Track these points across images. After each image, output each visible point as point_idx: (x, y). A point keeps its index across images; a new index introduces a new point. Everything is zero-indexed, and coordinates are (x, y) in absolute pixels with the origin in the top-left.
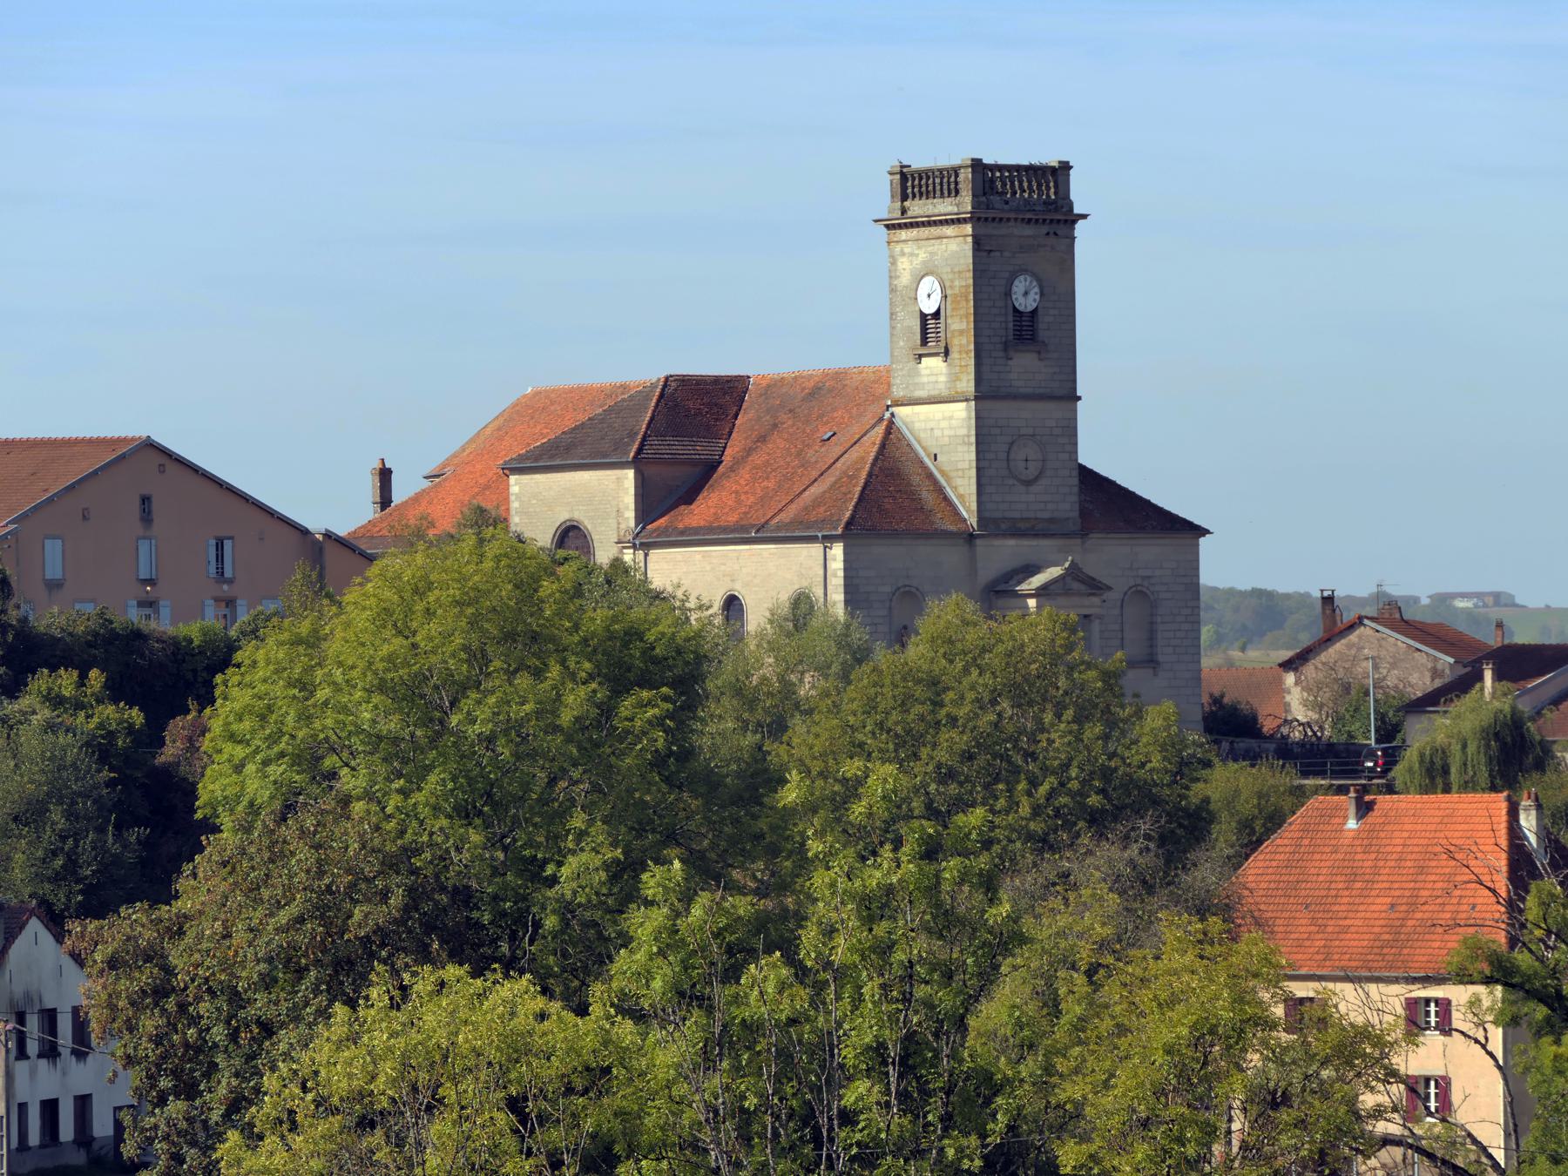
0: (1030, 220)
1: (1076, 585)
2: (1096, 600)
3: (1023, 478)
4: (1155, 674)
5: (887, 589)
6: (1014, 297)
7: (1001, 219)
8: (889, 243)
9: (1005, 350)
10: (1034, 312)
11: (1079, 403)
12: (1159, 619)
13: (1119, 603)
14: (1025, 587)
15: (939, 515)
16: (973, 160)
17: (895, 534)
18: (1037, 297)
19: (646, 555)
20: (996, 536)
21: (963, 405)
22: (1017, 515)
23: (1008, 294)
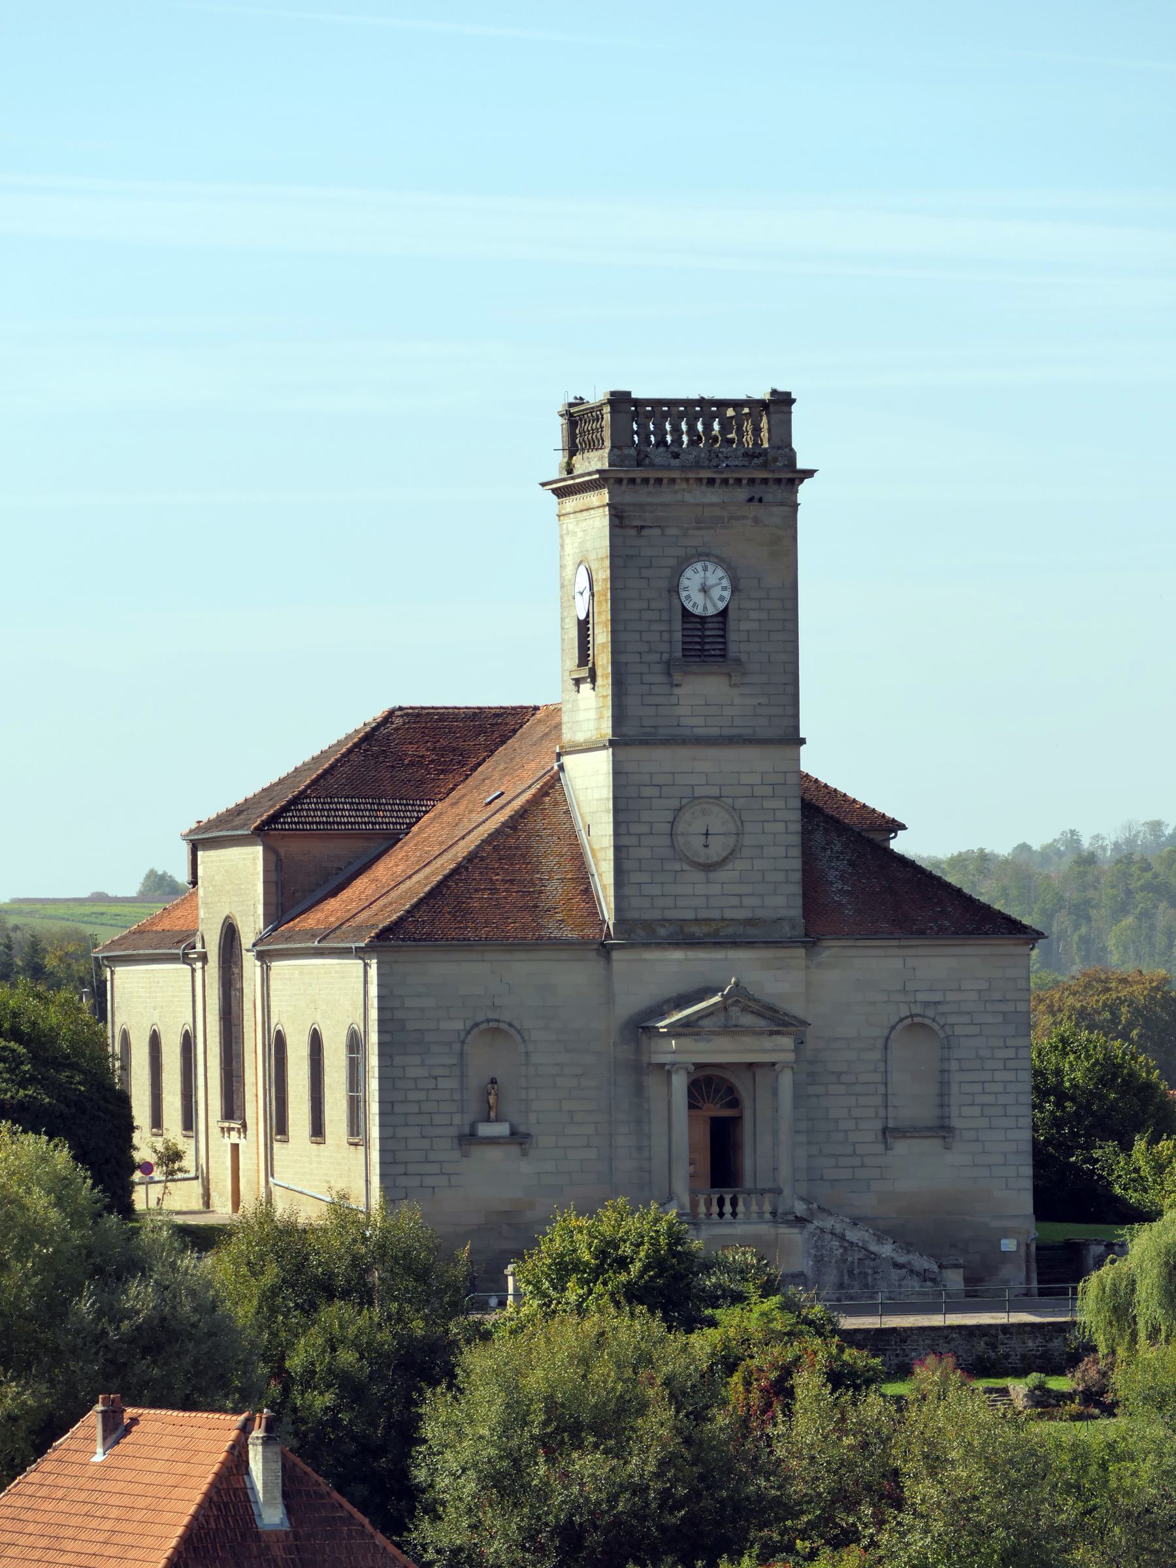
0: (711, 482)
1: (748, 1020)
2: (787, 1042)
3: (702, 860)
4: (524, 1154)
5: (460, 1026)
6: (683, 594)
7: (659, 481)
9: (669, 674)
10: (724, 613)
11: (803, 748)
12: (954, 1065)
13: (880, 1043)
15: (559, 917)
16: (613, 394)
17: (465, 944)
18: (727, 594)
19: (112, 973)
20: (646, 945)
21: (605, 752)
22: (689, 915)
23: (674, 589)
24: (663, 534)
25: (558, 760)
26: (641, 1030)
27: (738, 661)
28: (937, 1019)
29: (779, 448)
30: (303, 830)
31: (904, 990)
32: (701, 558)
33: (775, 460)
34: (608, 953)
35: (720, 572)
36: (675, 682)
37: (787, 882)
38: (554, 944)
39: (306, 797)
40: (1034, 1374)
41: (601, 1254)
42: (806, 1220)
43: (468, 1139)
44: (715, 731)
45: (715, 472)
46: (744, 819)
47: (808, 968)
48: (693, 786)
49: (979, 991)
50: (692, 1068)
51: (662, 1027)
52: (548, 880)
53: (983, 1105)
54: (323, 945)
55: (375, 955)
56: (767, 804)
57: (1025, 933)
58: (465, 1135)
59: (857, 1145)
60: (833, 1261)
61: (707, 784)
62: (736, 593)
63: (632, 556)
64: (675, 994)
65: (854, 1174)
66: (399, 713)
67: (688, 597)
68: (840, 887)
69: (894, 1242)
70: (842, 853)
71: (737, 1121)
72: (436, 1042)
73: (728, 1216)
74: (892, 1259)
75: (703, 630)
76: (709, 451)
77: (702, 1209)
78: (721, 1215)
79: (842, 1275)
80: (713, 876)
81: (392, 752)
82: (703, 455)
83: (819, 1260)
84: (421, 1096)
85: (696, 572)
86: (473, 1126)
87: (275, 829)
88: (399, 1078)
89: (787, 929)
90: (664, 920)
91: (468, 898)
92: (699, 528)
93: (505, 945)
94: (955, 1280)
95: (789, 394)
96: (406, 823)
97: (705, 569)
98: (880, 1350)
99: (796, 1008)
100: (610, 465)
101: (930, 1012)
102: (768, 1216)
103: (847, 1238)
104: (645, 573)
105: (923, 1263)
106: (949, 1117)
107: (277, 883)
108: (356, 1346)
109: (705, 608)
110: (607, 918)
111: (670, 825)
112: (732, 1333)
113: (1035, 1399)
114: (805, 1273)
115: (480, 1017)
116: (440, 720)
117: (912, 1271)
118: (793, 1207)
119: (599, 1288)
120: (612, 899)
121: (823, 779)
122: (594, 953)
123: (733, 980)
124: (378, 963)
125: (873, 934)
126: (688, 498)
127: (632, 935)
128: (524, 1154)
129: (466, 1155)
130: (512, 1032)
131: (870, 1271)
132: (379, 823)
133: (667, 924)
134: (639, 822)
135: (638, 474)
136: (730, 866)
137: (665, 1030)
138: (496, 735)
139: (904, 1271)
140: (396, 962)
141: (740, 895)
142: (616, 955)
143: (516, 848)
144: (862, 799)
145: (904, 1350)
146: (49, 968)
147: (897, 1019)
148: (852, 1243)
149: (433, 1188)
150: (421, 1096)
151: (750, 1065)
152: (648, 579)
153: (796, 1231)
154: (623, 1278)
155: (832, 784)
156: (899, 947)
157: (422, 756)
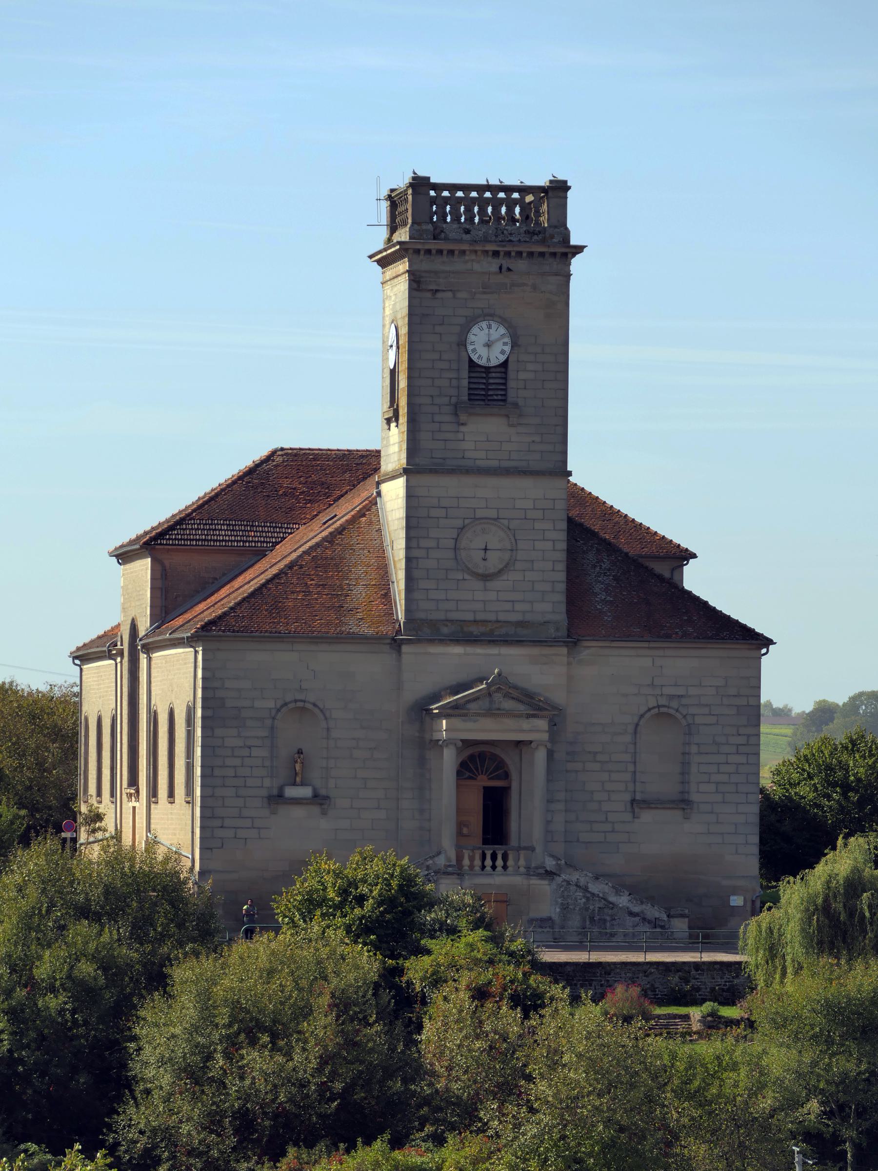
1: (509, 704)
2: (542, 724)
3: (480, 571)
5: (271, 704)
6: (470, 348)
7: (451, 252)
8: (382, 284)
9: (456, 415)
10: (505, 364)
12: (694, 749)
13: (631, 729)
14: (435, 708)
15: (359, 616)
17: (277, 637)
18: (507, 349)
20: (431, 641)
22: (469, 617)
23: (462, 344)
24: (454, 297)
25: (378, 487)
26: (425, 712)
27: (516, 405)
28: (681, 709)
29: (556, 227)
30: (184, 545)
31: (652, 685)
32: (486, 318)
33: (552, 237)
34: (400, 646)
35: (502, 330)
36: (461, 422)
37: (553, 591)
38: (352, 638)
39: (190, 519)
40: (708, 1003)
41: (344, 892)
42: (555, 874)
43: (277, 799)
44: (494, 463)
45: (498, 246)
46: (517, 538)
47: (569, 664)
48: (474, 509)
49: (717, 687)
50: (460, 744)
51: (436, 709)
52: (355, 585)
53: (717, 783)
54: (173, 636)
55: (201, 643)
56: (538, 525)
57: (757, 639)
58: (274, 796)
59: (609, 814)
60: (577, 909)
61: (487, 508)
62: (516, 348)
63: (427, 315)
64: (455, 683)
65: (605, 838)
66: (280, 453)
67: (474, 350)
68: (603, 597)
69: (630, 894)
70: (609, 570)
71: (506, 790)
72: (251, 718)
73: (488, 868)
74: (628, 908)
75: (487, 378)
76: (496, 229)
77: (466, 862)
78: (483, 867)
79: (584, 921)
80: (490, 584)
81: (269, 484)
82: (490, 232)
83: (565, 908)
84: (237, 762)
85: (482, 329)
86: (281, 789)
87: (161, 544)
88: (219, 747)
89: (553, 631)
90: (447, 620)
91: (284, 598)
92: (485, 293)
93: (311, 638)
94: (680, 926)
95: (566, 182)
96: (272, 542)
97: (489, 327)
98: (587, 980)
99: (559, 697)
100: (410, 238)
101: (674, 704)
102: (522, 870)
103: (590, 890)
104: (438, 329)
105: (654, 912)
106: (688, 793)
107: (162, 589)
108: (93, 958)
109: (489, 360)
110: (400, 617)
111: (454, 541)
112: (441, 959)
113: (707, 1024)
115: (289, 698)
116: (314, 459)
117: (644, 919)
119: (339, 921)
120: (403, 602)
121: (631, 515)
122: (388, 647)
123: (496, 671)
124: (203, 650)
125: (628, 637)
126: (477, 267)
127: (419, 632)
128: (324, 813)
129: (274, 813)
130: (316, 710)
131: (608, 918)
132: (249, 542)
133: (449, 624)
134: (428, 537)
135: (433, 245)
136: (505, 577)
137: (437, 711)
138: (360, 472)
139: (637, 919)
140: (218, 649)
141: (513, 601)
142: (405, 648)
143: (332, 559)
144: (661, 532)
145: (608, 981)
147: (646, 709)
148: (593, 894)
149: (246, 839)
150: (237, 762)
151: (518, 743)
152: (441, 334)
153: (546, 882)
154: (358, 911)
155: (639, 520)
156: (649, 648)
157: (294, 489)
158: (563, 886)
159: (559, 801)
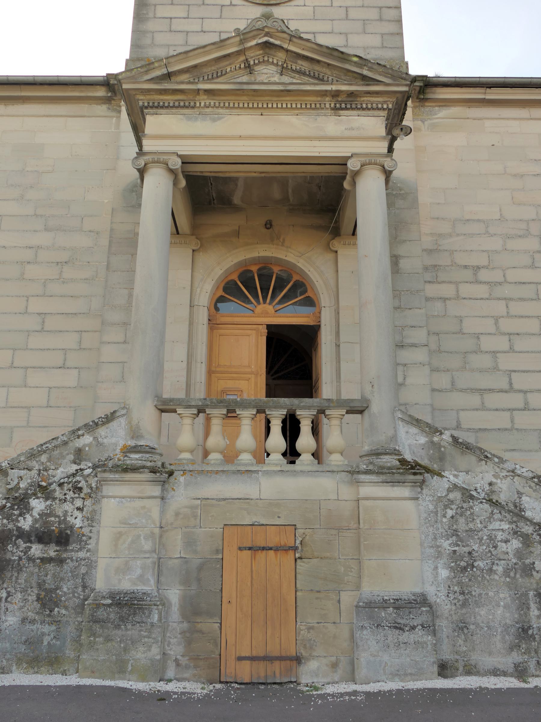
37: (381, 20)
42: (428, 470)
59: (513, 374)
79: (524, 606)
114: (432, 598)
118: (394, 438)
146: (82, 637)
153: (405, 491)
158: (452, 502)
159: (414, 345)
